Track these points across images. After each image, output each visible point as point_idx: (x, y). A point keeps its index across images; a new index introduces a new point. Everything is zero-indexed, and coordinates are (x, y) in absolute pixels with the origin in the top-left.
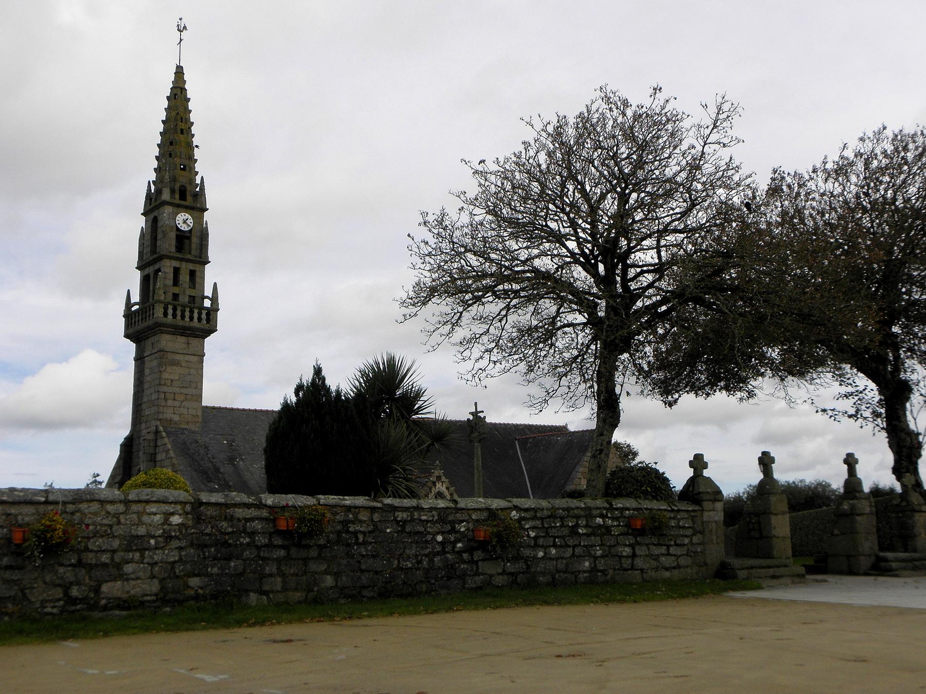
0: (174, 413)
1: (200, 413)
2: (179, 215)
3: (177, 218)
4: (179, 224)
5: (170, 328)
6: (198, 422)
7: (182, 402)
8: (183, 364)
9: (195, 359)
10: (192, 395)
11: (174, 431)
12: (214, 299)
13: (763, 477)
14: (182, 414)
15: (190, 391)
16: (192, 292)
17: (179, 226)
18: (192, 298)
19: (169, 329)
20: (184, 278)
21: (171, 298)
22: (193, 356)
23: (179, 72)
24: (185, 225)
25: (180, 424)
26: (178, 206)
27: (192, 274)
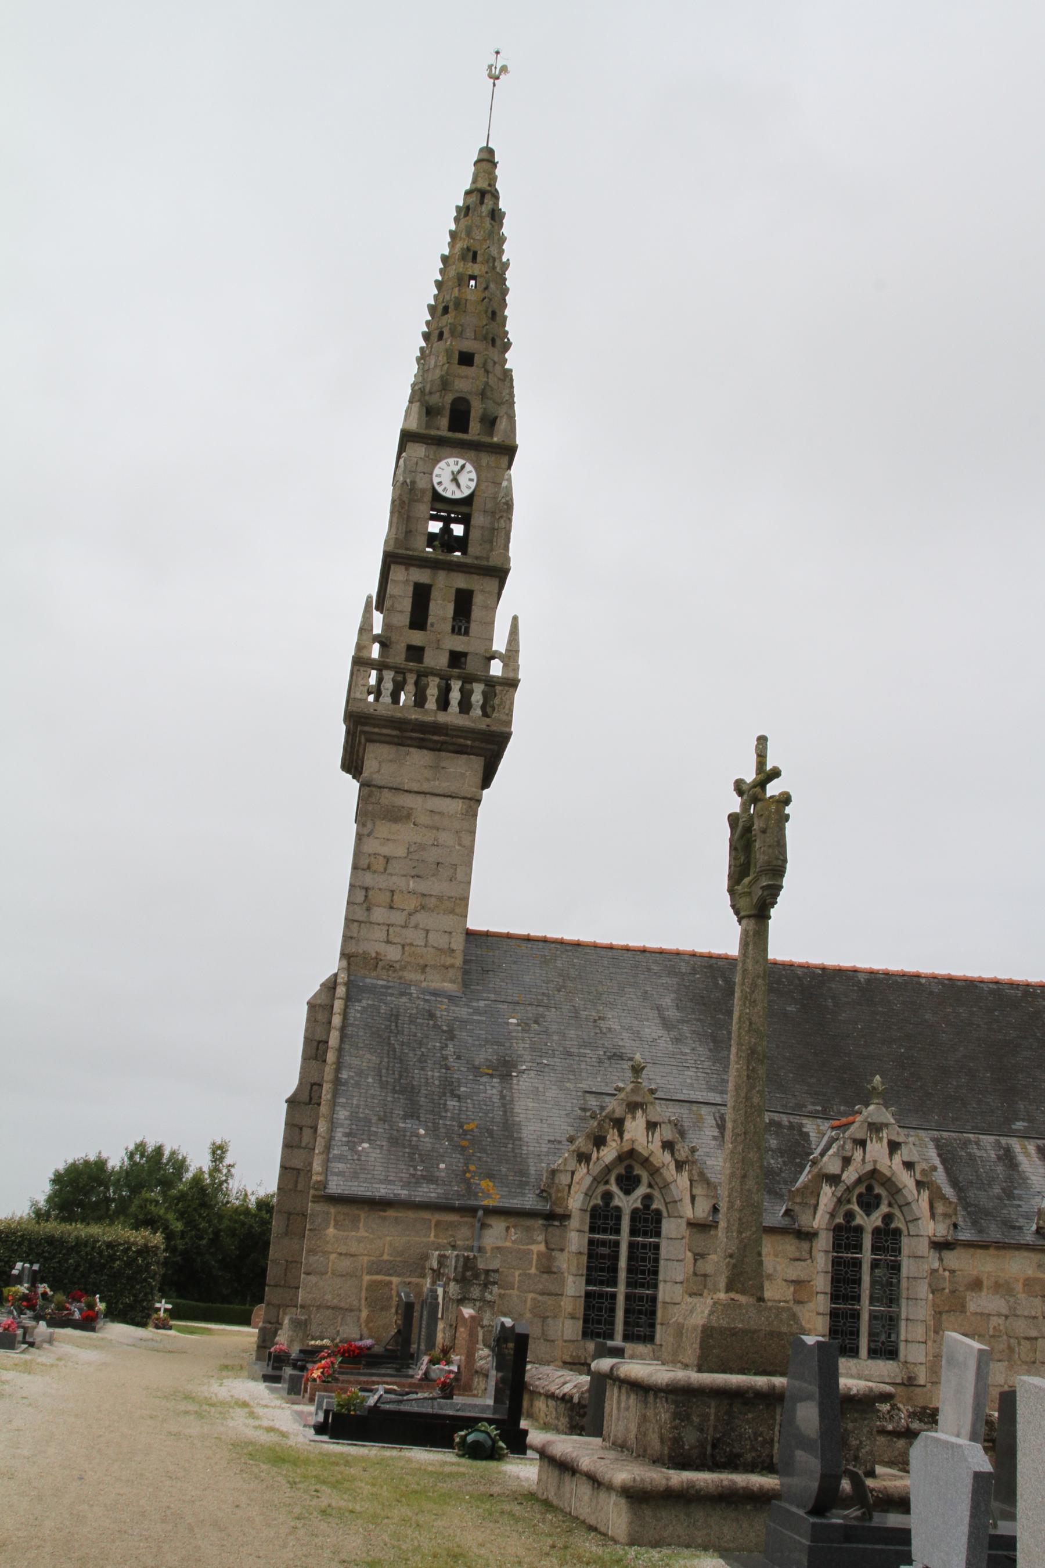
0: (388, 942)
1: (458, 943)
2: (442, 464)
3: (437, 471)
4: (440, 483)
5: (385, 727)
6: (452, 966)
7: (410, 914)
8: (423, 819)
9: (455, 806)
10: (440, 898)
11: (382, 986)
12: (511, 656)
13: (799, 1405)
14: (411, 944)
15: (434, 886)
16: (458, 643)
17: (440, 489)
18: (457, 658)
19: (385, 731)
20: (441, 609)
21: (403, 656)
22: (448, 800)
23: (487, 160)
24: (452, 487)
25: (403, 968)
26: (440, 442)
27: (463, 603)
